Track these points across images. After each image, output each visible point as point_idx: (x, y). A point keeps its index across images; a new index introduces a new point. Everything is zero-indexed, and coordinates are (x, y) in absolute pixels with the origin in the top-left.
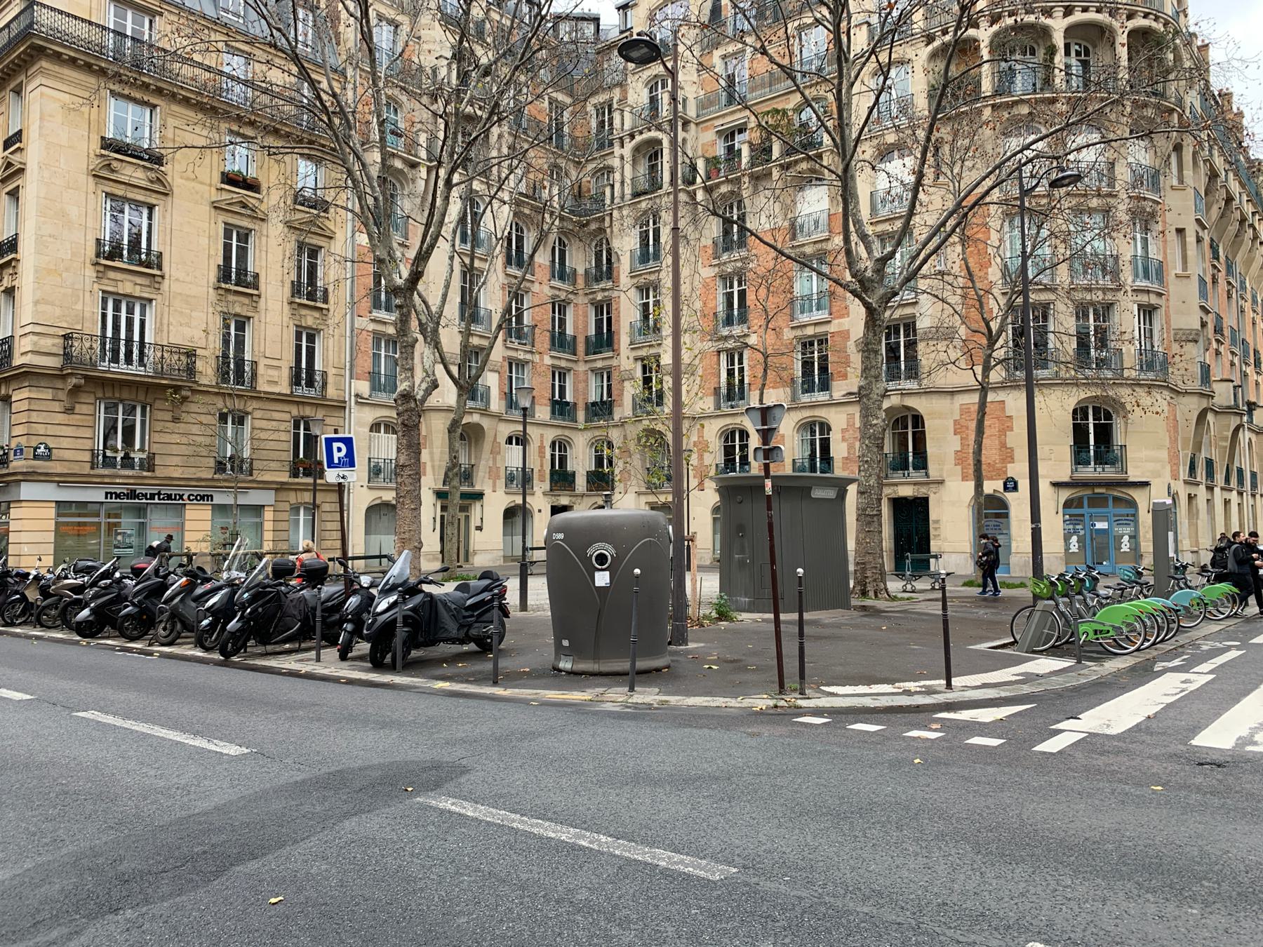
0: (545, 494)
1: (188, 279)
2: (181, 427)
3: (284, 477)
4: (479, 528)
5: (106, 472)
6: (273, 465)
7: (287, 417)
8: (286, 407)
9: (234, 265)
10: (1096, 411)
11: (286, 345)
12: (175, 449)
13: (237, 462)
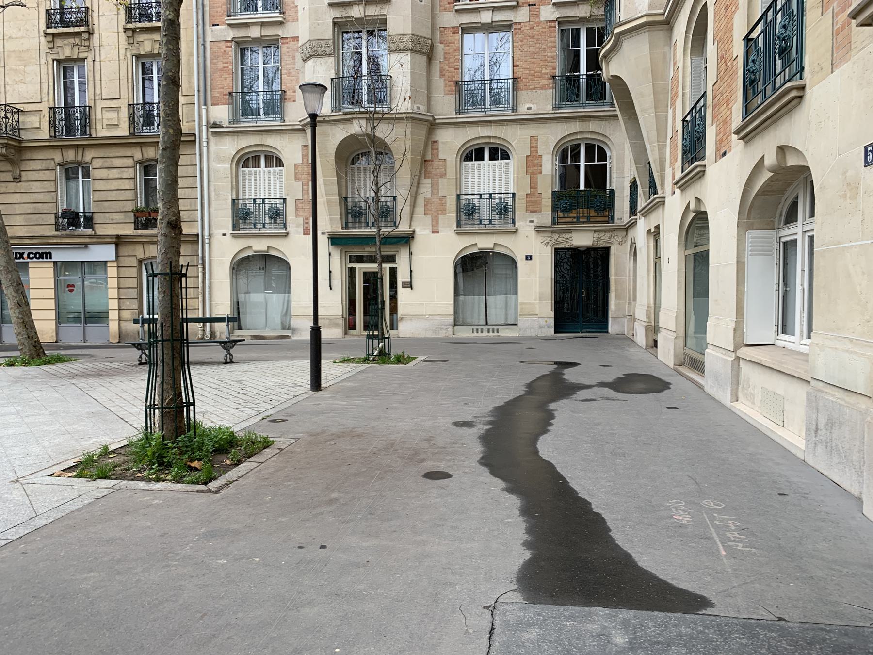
0: (540, 230)
1: (20, 34)
2: (22, 186)
3: (128, 230)
4: (409, 285)
6: (117, 217)
7: (129, 162)
8: (128, 152)
10: (590, 148)
11: (124, 82)
12: (19, 209)
13: (71, 218)
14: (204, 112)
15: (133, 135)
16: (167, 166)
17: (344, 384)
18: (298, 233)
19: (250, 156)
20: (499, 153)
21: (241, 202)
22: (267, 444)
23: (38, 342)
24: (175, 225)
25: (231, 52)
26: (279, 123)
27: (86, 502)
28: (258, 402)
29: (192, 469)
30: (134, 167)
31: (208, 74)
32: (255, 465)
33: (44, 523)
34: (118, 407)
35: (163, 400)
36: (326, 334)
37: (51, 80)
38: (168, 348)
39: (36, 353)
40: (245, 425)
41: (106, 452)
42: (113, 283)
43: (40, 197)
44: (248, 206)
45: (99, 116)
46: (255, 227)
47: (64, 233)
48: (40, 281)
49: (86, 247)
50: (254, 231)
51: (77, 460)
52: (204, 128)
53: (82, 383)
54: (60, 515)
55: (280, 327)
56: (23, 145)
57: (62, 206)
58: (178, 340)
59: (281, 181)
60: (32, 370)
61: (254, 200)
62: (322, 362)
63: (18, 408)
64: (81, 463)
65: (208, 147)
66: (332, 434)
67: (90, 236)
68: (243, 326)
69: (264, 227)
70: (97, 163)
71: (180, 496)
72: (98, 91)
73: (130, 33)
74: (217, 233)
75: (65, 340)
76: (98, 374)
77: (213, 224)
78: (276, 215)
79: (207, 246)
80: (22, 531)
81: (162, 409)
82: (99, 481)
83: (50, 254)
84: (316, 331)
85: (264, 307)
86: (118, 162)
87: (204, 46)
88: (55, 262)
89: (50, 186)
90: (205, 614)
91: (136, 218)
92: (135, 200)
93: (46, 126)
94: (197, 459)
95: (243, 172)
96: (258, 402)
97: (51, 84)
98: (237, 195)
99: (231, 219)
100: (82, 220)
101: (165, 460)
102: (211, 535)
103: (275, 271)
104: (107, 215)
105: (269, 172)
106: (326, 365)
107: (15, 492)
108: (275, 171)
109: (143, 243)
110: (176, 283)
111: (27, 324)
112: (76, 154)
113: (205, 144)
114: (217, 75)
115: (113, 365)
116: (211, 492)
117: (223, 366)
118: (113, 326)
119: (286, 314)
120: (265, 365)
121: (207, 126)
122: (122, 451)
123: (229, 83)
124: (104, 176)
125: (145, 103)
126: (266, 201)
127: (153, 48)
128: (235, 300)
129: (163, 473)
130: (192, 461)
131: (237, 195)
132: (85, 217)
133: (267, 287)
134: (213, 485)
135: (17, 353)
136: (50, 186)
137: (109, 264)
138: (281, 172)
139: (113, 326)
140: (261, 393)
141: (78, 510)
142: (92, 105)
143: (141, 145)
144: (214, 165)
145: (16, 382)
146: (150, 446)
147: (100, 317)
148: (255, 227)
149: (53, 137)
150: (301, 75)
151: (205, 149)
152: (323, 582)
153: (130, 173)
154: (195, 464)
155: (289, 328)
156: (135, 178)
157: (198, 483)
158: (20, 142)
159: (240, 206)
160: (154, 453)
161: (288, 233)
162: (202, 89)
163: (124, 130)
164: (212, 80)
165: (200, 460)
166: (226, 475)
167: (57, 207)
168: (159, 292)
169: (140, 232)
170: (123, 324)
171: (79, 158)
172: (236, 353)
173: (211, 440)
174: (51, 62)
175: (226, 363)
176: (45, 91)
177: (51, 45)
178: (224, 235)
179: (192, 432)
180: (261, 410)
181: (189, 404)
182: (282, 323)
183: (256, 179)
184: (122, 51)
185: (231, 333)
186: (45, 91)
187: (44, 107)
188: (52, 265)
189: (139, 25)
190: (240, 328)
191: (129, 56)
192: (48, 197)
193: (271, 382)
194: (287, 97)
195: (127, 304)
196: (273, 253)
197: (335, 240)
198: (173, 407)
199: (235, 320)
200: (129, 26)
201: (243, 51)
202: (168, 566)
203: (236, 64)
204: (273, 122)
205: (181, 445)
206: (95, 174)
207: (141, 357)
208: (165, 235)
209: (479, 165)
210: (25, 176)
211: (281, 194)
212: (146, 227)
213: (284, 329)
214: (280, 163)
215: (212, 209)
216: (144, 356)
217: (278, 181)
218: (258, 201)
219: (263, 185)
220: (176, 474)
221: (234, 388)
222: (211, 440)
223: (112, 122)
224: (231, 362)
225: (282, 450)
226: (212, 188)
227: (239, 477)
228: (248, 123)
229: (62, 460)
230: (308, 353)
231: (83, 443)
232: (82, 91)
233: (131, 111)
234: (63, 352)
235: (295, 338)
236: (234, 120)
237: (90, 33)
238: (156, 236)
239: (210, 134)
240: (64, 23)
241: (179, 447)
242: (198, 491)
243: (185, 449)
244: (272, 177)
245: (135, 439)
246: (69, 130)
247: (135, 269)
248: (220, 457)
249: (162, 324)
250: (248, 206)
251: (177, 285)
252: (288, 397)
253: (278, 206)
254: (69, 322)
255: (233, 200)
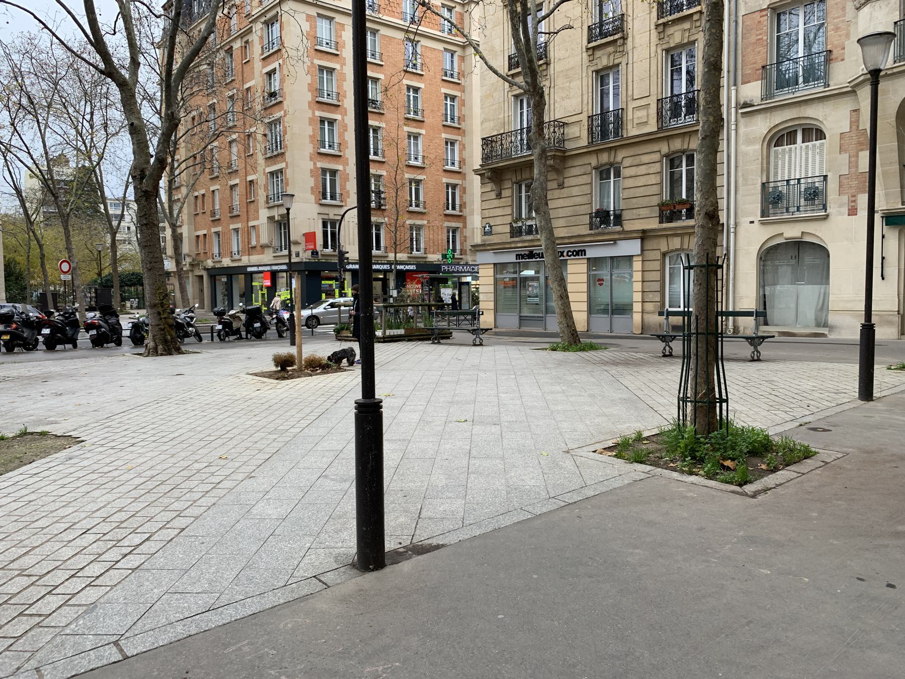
3: (653, 224)
5: (530, 237)
6: (644, 212)
7: (656, 157)
8: (655, 147)
9: (327, 140)
11: (654, 79)
13: (603, 216)
14: (733, 93)
15: (660, 129)
16: (706, 156)
17: (900, 396)
18: (841, 214)
19: (785, 132)
20: (814, 133)
21: (772, 185)
22: (807, 454)
23: (575, 330)
24: (712, 216)
25: (766, 21)
26: (822, 89)
27: (626, 482)
28: (792, 406)
29: (724, 467)
30: (661, 161)
31: (740, 52)
32: (795, 475)
33: (593, 493)
34: (655, 397)
35: (696, 394)
36: (882, 334)
37: (590, 90)
38: (702, 340)
39: (573, 341)
40: (780, 429)
41: (639, 438)
42: (637, 276)
43: (578, 200)
44: (780, 189)
45: (630, 117)
46: (787, 211)
47: (596, 231)
48: (576, 274)
49: (615, 243)
50: (786, 216)
51: (615, 441)
52: (733, 110)
53: (614, 370)
54: (604, 489)
55: (813, 323)
56: (567, 154)
57: (596, 207)
58: (712, 334)
59: (821, 155)
60: (571, 355)
61: (788, 181)
62: (876, 367)
63: (564, 388)
64: (619, 444)
65: (736, 130)
66: (893, 455)
67: (619, 233)
68: (769, 322)
69: (798, 210)
70: (627, 162)
71: (714, 493)
72: (630, 93)
73: (661, 29)
74: (744, 221)
75: (595, 330)
76: (626, 363)
77: (739, 211)
78: (814, 195)
79: (732, 235)
80: (576, 498)
81: (695, 402)
82: (636, 464)
83: (585, 251)
84: (868, 330)
85: (795, 301)
86: (645, 159)
87: (736, 22)
88: (588, 259)
89: (586, 189)
90: (751, 622)
91: (661, 211)
92: (661, 194)
93: (585, 134)
94: (730, 458)
95: (775, 151)
96: (792, 406)
97: (590, 94)
98: (768, 177)
99: (759, 205)
100: (612, 218)
101: (698, 454)
102: (751, 540)
103: (808, 259)
104: (635, 211)
105: (807, 147)
106: (879, 372)
107: (567, 462)
108: (814, 146)
109: (667, 236)
110: (712, 275)
111: (567, 314)
112: (683, 142)
113: (733, 127)
114: (749, 50)
115: (639, 355)
116: (747, 495)
117: (749, 364)
118: (637, 318)
119: (822, 308)
120: (797, 366)
121: (736, 108)
122: (655, 439)
123: (763, 55)
124: (633, 174)
125: (672, 96)
126: (802, 181)
127: (682, 39)
128: (761, 293)
129: (695, 467)
130: (725, 459)
131: (768, 177)
132: (615, 215)
133: (796, 279)
134: (749, 488)
135: (559, 340)
136: (586, 189)
137: (635, 259)
138: (822, 145)
139: (637, 318)
140: (796, 396)
141: (620, 488)
142: (625, 107)
143: (668, 138)
144: (743, 148)
145: (560, 365)
146: (683, 438)
147: (624, 309)
148: (787, 211)
149: (591, 143)
150: (852, 29)
151: (733, 133)
152: (893, 626)
153: (656, 167)
154: (728, 463)
155: (825, 325)
156: (661, 172)
157: (731, 483)
158: (564, 152)
159: (771, 190)
160: (686, 446)
161: (828, 216)
162: (732, 69)
163: (652, 127)
164: (743, 56)
165: (733, 460)
166: (763, 480)
167: (592, 207)
168: (694, 285)
169: (665, 225)
170: (646, 316)
171: (612, 160)
172: (765, 350)
173: (744, 440)
174: (590, 74)
175: (753, 360)
176: (585, 102)
177: (591, 58)
178: (752, 222)
179: (724, 430)
180: (798, 415)
181: (722, 401)
182: (816, 319)
183: (790, 157)
184: (653, 48)
185: (757, 328)
186: (585, 102)
187: (584, 117)
188: (586, 261)
189: (670, 18)
190: (766, 324)
191: (659, 51)
192: (585, 200)
193: (807, 385)
194: (833, 57)
195: (650, 297)
196: (807, 239)
197: (891, 219)
198: (705, 402)
199: (761, 315)
200: (661, 21)
201: (779, 15)
202: (708, 561)
203: (772, 33)
204: (816, 89)
205: (713, 441)
206: (625, 172)
207: (664, 349)
208: (702, 227)
209: (790, 150)
210: (567, 182)
211: (821, 169)
212: (670, 220)
213: (818, 325)
214: (820, 135)
215: (739, 196)
216: (667, 348)
217: (817, 157)
218: (792, 182)
219: (800, 163)
220: (709, 470)
221: (763, 388)
222: (744, 440)
223: (641, 120)
224: (759, 360)
225: (827, 463)
226: (740, 174)
227: (777, 485)
228: (785, 96)
229: (602, 439)
230: (856, 354)
231: (619, 426)
232: (616, 95)
233: (660, 106)
234: (594, 341)
235: (832, 337)
236: (767, 95)
237: (624, 38)
238: (693, 227)
239: (739, 115)
240: (603, 35)
241: (708, 443)
242: (733, 492)
243: (717, 446)
244: (810, 152)
245: (667, 429)
246: (604, 134)
247: (658, 262)
248: (755, 460)
249: (697, 317)
250: (780, 189)
251: (713, 278)
252: (829, 404)
253: (817, 185)
254: (598, 313)
255: (763, 184)
